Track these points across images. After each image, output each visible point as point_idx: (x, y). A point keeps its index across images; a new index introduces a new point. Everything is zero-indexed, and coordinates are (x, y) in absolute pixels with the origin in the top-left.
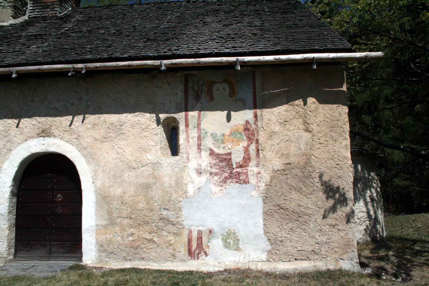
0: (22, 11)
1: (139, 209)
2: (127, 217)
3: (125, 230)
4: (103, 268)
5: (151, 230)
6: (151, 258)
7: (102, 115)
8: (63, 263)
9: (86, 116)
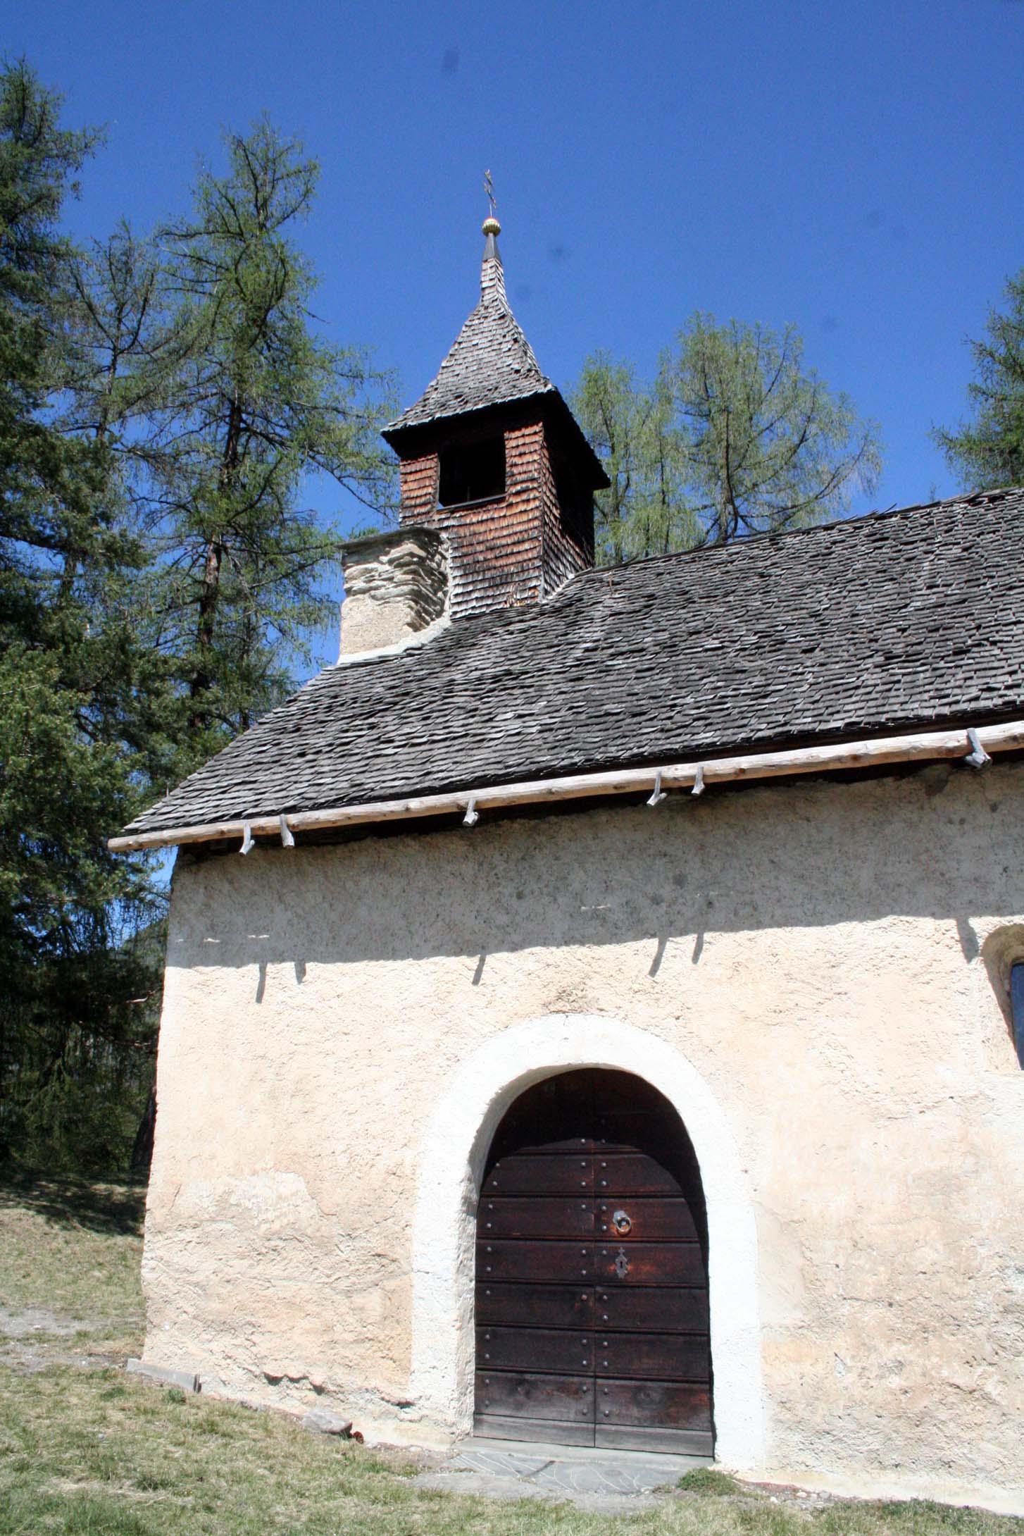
0: (435, 603)
1: (921, 1268)
2: (877, 1300)
3: (870, 1349)
4: (795, 1490)
5: (971, 1352)
6: (980, 1463)
7: (760, 932)
8: (650, 1462)
9: (707, 936)
